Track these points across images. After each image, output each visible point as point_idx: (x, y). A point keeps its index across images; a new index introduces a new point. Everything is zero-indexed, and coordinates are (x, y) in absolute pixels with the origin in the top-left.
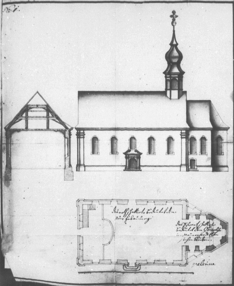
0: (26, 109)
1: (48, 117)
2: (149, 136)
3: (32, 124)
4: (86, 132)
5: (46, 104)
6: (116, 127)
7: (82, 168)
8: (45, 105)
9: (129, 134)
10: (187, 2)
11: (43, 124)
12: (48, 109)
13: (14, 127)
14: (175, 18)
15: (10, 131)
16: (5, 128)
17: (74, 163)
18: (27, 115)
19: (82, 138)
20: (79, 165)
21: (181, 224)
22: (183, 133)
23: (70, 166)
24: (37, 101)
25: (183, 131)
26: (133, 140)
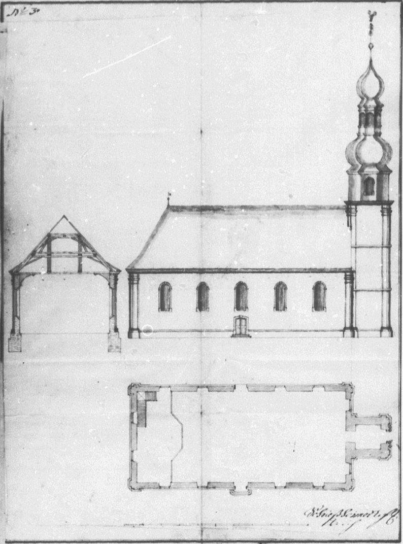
0: (49, 239)
1: (49, 253)
2: (277, 281)
3: (58, 264)
4: (141, 276)
5: (76, 232)
6: (175, 267)
7: (135, 334)
8: (75, 234)
9: (232, 280)
10: (179, 2)
11: (73, 263)
12: (79, 238)
13: (26, 269)
14: (373, 112)
15: (17, 277)
16: (11, 272)
17: (124, 328)
18: (49, 249)
19: (135, 284)
20: (131, 330)
21: (348, 412)
22: (348, 275)
23: (116, 330)
24: (64, 228)
25: (348, 274)
26: (167, 288)
